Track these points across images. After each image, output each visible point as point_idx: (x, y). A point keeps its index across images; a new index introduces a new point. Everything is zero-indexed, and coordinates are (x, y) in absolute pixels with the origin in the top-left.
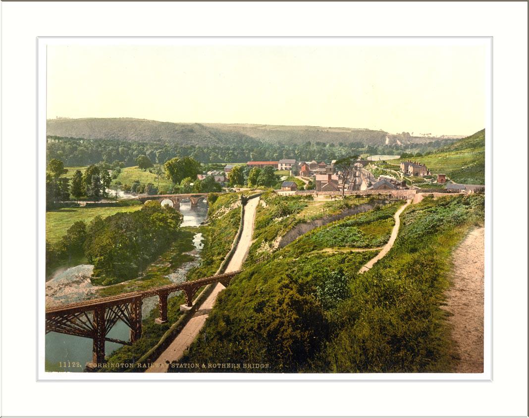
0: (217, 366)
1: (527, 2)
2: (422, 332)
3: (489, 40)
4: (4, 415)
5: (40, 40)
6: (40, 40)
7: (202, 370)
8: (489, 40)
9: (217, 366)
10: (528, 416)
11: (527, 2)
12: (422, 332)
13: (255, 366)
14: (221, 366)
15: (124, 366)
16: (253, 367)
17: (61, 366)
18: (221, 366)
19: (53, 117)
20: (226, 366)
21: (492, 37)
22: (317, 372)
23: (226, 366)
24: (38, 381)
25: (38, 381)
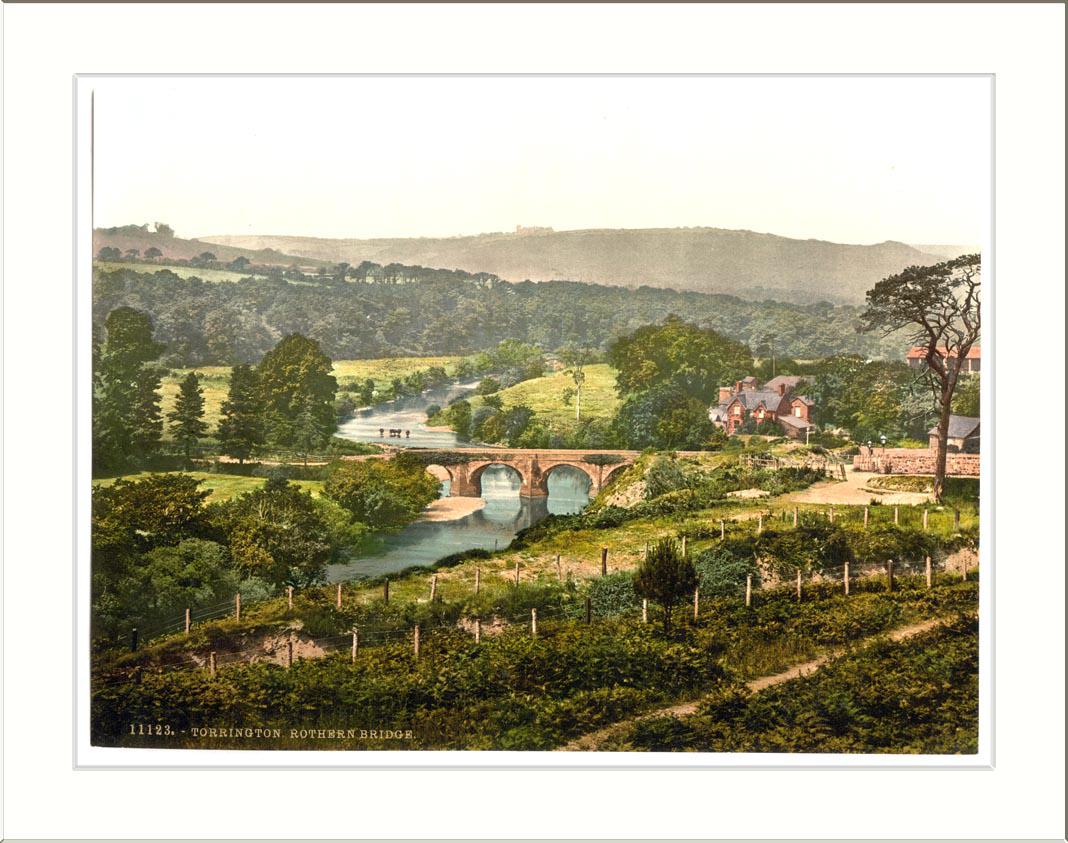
0: (309, 736)
1: (1063, 5)
2: (894, 673)
3: (988, 80)
4: (9, 835)
5: (80, 80)
6: (80, 80)
7: (241, 744)
8: (988, 80)
9: (309, 736)
10: (1066, 838)
11: (1063, 5)
12: (894, 673)
13: (384, 735)
14: (316, 735)
15: (261, 735)
16: (231, 736)
17: (133, 733)
18: (316, 735)
19: (106, 222)
20: (327, 735)
21: (994, 74)
22: (93, 664)
23: (327, 735)
24: (76, 767)
25: (76, 767)
